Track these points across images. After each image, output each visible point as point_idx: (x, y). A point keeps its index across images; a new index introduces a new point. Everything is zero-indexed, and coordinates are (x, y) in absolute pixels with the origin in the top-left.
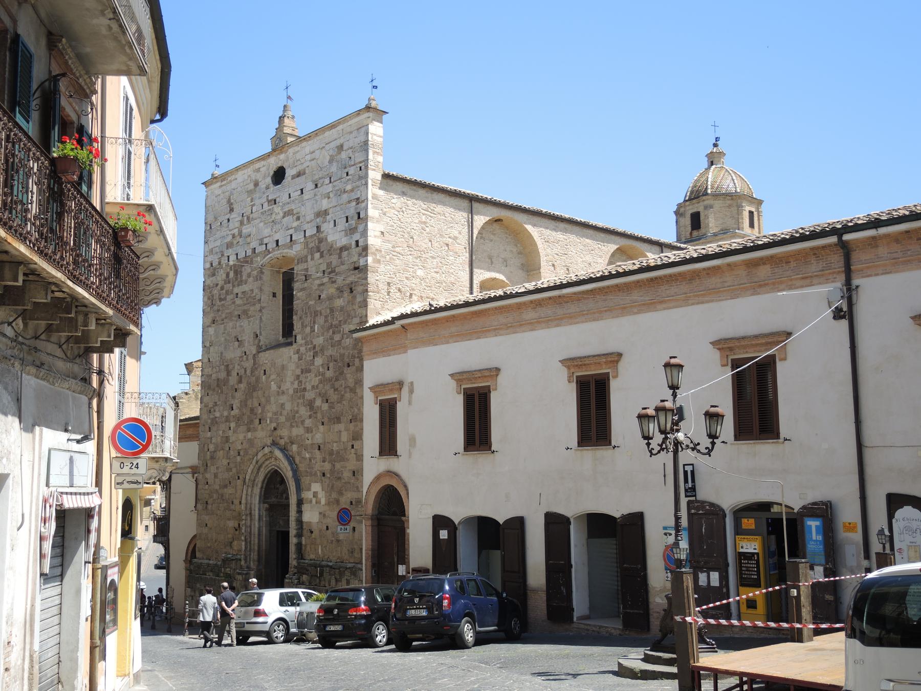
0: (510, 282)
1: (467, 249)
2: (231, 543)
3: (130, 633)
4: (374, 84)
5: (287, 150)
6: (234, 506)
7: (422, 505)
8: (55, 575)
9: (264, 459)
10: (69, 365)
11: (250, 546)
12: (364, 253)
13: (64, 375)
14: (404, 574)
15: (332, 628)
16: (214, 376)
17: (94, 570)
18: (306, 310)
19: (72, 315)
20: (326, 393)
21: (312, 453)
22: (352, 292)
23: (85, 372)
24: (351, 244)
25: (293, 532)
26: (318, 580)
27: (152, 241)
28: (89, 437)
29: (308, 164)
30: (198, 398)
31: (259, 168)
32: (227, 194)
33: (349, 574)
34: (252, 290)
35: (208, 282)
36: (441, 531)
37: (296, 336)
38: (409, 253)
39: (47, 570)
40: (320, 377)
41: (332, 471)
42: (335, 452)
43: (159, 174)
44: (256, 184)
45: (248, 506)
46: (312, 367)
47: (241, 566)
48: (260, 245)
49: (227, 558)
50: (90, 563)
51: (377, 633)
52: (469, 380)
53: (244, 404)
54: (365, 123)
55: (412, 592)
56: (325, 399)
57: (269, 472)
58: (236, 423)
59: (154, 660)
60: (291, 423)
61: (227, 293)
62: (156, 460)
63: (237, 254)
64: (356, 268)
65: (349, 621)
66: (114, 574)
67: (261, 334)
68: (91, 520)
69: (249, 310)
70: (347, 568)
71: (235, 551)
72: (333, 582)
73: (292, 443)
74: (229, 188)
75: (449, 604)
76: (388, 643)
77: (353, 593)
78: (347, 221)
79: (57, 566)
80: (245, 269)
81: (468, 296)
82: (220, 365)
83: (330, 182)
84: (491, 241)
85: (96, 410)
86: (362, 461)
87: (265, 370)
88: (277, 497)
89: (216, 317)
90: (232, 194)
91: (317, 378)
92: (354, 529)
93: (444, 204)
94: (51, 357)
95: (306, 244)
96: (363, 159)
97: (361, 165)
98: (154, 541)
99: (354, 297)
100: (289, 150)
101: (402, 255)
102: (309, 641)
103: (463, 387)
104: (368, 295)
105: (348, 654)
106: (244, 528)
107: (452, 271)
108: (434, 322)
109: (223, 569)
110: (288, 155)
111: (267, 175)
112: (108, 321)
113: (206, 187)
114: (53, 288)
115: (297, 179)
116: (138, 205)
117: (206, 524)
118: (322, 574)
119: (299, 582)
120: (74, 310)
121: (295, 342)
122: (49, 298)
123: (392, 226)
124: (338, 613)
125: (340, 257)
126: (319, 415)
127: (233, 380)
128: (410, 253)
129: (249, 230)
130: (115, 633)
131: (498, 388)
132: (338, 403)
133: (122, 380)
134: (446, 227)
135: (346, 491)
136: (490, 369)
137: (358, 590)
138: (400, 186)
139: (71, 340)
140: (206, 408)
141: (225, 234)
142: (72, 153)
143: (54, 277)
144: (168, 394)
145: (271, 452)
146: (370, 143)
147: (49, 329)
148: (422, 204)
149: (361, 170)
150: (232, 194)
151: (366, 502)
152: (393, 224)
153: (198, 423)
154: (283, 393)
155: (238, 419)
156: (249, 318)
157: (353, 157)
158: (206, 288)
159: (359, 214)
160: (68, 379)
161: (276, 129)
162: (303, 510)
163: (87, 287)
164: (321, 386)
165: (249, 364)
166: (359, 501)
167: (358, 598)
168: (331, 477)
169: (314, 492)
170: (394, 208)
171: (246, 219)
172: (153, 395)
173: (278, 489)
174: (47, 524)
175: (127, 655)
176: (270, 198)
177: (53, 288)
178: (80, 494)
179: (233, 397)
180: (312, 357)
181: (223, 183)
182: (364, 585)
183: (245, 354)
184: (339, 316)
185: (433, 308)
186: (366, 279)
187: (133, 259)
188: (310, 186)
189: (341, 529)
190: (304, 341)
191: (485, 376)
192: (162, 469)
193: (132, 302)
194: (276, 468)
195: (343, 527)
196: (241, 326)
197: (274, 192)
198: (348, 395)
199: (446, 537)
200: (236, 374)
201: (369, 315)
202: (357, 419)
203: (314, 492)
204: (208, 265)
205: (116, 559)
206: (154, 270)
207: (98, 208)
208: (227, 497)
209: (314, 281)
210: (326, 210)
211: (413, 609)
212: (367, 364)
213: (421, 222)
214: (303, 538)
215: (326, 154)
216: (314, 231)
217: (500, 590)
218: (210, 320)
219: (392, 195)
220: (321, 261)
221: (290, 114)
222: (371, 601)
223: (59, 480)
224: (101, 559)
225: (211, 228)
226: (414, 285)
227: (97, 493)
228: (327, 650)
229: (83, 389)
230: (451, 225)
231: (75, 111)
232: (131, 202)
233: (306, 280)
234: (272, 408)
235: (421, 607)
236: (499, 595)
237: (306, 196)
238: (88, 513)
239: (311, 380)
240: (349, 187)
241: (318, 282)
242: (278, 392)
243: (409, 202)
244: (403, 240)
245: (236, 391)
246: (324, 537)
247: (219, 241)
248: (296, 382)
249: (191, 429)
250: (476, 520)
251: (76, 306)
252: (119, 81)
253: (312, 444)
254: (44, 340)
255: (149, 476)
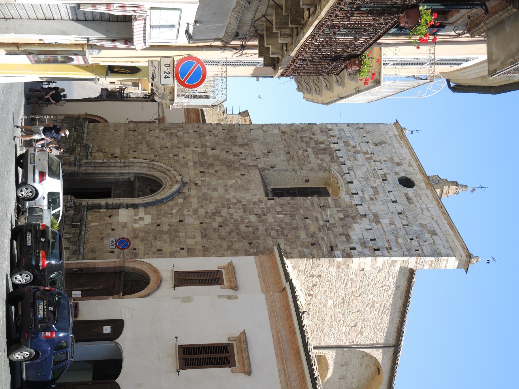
0: (326, 382)
1: (352, 344)
2: (101, 151)
3: (28, 74)
4: (491, 261)
5: (429, 189)
6: (132, 152)
7: (132, 310)
8: (78, 15)
9: (171, 175)
10: (249, 22)
11: (99, 167)
12: (345, 254)
13: (241, 19)
14: (74, 296)
15: (29, 237)
16: (239, 134)
17: (82, 45)
18: (295, 207)
19: (290, 25)
20: (226, 225)
21: (177, 215)
22: (313, 245)
23: (243, 35)
24: (352, 243)
25: (110, 201)
26: (69, 223)
27: (350, 84)
28: (191, 40)
29: (418, 206)
30: (220, 121)
31: (412, 166)
32: (389, 141)
33: (74, 249)
34: (310, 163)
35: (315, 128)
36: (109, 327)
37: (273, 199)
38: (347, 293)
39: (82, 9)
40: (240, 220)
41: (161, 232)
42: (177, 234)
43: (406, 88)
44: (398, 164)
45: (132, 164)
46: (248, 213)
47: (82, 160)
48: (348, 168)
49: (89, 148)
50: (88, 41)
51: (23, 275)
52: (241, 348)
53: (217, 158)
54: (456, 254)
55: (58, 304)
56: (222, 224)
57: (160, 180)
58: (201, 153)
59: (5, 92)
60: (201, 197)
61: (307, 143)
62: (172, 92)
63: (339, 150)
64: (332, 248)
65: (34, 251)
66: (78, 61)
67: (274, 171)
68: (123, 42)
69: (294, 161)
70: (79, 247)
71: (95, 155)
72: (67, 236)
73: (185, 199)
74: (395, 142)
75: (47, 337)
76: (15, 285)
77: (59, 253)
78: (371, 240)
79: (85, 16)
80: (327, 157)
81: (312, 345)
82: (248, 139)
83: (404, 225)
84: (361, 365)
85: (212, 44)
86: (170, 257)
87: (244, 175)
88: (139, 187)
89: (287, 134)
90: (390, 144)
91: (239, 218)
92: (113, 252)
93: (390, 323)
94: (255, 9)
95: (350, 206)
96: (425, 252)
97: (420, 251)
98: (102, 89)
99: (307, 247)
100: (429, 191)
101: (345, 287)
102: (17, 218)
103: (234, 343)
104: (310, 258)
105: (6, 251)
106: (114, 161)
107: (333, 330)
108: (290, 316)
109: (79, 145)
110: (424, 189)
111: (407, 173)
112: (286, 52)
113: (394, 124)
114: (312, 10)
115: (405, 197)
116: (380, 73)
117: (117, 131)
118: (74, 226)
119: (68, 208)
120: (294, 26)
121: (268, 199)
122: (303, 7)
123: (369, 278)
124: (41, 241)
125: (341, 234)
126: (208, 220)
127: (236, 149)
128: (347, 294)
129: (360, 159)
130: (29, 62)
131: (234, 374)
132: (219, 235)
133: (237, 64)
134: (370, 324)
135: (145, 244)
136: (250, 367)
137: (61, 257)
138: (404, 284)
139: (269, 23)
140: (212, 128)
141: (356, 140)
142: (423, 21)
143: (321, 10)
144: (226, 100)
145: (177, 181)
146: (440, 258)
147: (278, 7)
148: (390, 303)
149: (416, 250)
150: (390, 144)
151: (135, 262)
152: (371, 279)
153: (200, 122)
154: (226, 190)
155: (204, 154)
156: (288, 161)
157: (426, 243)
158: (311, 126)
159: (378, 250)
160: (238, 22)
161: (446, 180)
162: (129, 209)
163: (313, 36)
164: (233, 221)
165: (249, 161)
166: (136, 255)
167: (54, 258)
168: (156, 232)
169: (143, 218)
170: (385, 279)
171: (369, 157)
172: (224, 88)
173: (147, 188)
174: (120, 8)
175: (10, 72)
176: (387, 175)
177: (312, 10)
178: (145, 34)
179: (222, 150)
180: (256, 213)
181: (398, 137)
182: (65, 262)
183: (257, 159)
184: (291, 235)
185: (301, 315)
186: (323, 257)
187: (336, 71)
188: (400, 209)
189: (112, 241)
190: (269, 206)
191: (243, 362)
192: (164, 97)
193: (301, 70)
194: (164, 186)
195: (114, 243)
196: (280, 155)
197: (392, 179)
198: (225, 244)
199: (104, 332)
200: (241, 152)
201: (293, 259)
202: (206, 251)
203: (143, 218)
204: (329, 127)
205: (90, 62)
206: (327, 86)
207: (379, 41)
208: (139, 147)
209: (320, 213)
210: (380, 222)
211: (44, 306)
212: (252, 259)
213: (374, 302)
214: (105, 210)
215: (428, 221)
216: (362, 213)
217: (58, 381)
218: (284, 129)
219: (396, 277)
220: (337, 218)
221: (460, 190)
222: (51, 269)
223: (156, 18)
224: (91, 50)
225: (360, 128)
226: (319, 297)
227: (145, 47)
228: (10, 233)
229: (230, 34)
230: (373, 329)
231: (457, 21)
232: (383, 66)
233: (320, 207)
234: (214, 182)
235: (45, 313)
236: (53, 381)
237: (391, 205)
238: (128, 40)
239: (237, 212)
240: (400, 241)
241: (319, 216)
242: (227, 186)
243: (391, 292)
244: (358, 287)
245: (227, 152)
246: (106, 227)
247: (350, 135)
248: (235, 201)
249: (195, 117)
250: (119, 358)
251: (297, 28)
252: (482, 54)
253: (184, 215)
254: (269, 3)
255: (159, 87)
